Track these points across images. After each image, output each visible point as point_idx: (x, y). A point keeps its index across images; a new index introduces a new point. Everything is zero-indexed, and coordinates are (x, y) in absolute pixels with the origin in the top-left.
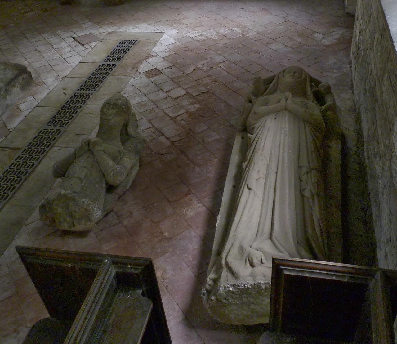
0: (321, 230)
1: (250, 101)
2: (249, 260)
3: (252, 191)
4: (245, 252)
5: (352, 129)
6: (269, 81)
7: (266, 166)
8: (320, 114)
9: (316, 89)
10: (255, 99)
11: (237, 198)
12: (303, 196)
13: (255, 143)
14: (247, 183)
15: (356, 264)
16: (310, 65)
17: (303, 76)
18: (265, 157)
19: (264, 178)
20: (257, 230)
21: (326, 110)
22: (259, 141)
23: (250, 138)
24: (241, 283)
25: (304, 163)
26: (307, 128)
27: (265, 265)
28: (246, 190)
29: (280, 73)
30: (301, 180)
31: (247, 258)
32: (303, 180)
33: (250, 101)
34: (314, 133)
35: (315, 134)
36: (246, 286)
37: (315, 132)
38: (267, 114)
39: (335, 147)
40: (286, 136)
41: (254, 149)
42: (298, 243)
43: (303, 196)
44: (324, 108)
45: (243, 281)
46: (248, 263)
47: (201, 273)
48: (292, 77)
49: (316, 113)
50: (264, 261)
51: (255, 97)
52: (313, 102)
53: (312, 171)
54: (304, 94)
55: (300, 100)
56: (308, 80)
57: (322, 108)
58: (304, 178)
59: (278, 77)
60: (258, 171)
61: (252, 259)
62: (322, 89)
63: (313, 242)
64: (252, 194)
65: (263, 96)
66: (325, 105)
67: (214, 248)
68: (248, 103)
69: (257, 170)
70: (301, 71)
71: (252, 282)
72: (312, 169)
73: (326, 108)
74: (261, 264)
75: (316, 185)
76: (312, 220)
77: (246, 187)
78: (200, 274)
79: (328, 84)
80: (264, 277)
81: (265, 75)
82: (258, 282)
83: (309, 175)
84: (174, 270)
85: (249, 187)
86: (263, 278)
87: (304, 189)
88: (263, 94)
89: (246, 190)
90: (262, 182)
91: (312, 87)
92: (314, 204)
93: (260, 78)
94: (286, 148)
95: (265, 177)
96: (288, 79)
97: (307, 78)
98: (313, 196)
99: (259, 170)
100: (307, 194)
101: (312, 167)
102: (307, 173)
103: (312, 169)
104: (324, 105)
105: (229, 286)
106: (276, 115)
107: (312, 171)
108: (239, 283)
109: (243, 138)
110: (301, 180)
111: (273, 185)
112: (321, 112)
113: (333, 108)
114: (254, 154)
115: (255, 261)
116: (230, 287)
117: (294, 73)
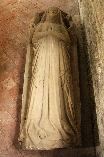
0: (72, 106)
2: (39, 135)
4: (37, 130)
5: (80, 35)
9: (64, 18)
14: (35, 84)
17: (58, 13)
20: (42, 108)
21: (71, 30)
25: (63, 68)
27: (47, 138)
31: (38, 134)
32: (63, 79)
33: (33, 26)
34: (65, 47)
37: (66, 46)
38: (42, 37)
42: (62, 119)
46: (38, 137)
47: (18, 120)
50: (46, 136)
54: (59, 22)
57: (68, 29)
58: (63, 78)
62: (68, 18)
64: (37, 89)
75: (69, 81)
77: (34, 85)
78: (18, 120)
80: (47, 145)
83: (65, 75)
84: (6, 119)
88: (39, 23)
90: (42, 82)
91: (62, 16)
94: (53, 58)
100: (65, 88)
102: (64, 74)
111: (47, 95)
113: (73, 29)
115: (42, 137)
117: (54, 11)
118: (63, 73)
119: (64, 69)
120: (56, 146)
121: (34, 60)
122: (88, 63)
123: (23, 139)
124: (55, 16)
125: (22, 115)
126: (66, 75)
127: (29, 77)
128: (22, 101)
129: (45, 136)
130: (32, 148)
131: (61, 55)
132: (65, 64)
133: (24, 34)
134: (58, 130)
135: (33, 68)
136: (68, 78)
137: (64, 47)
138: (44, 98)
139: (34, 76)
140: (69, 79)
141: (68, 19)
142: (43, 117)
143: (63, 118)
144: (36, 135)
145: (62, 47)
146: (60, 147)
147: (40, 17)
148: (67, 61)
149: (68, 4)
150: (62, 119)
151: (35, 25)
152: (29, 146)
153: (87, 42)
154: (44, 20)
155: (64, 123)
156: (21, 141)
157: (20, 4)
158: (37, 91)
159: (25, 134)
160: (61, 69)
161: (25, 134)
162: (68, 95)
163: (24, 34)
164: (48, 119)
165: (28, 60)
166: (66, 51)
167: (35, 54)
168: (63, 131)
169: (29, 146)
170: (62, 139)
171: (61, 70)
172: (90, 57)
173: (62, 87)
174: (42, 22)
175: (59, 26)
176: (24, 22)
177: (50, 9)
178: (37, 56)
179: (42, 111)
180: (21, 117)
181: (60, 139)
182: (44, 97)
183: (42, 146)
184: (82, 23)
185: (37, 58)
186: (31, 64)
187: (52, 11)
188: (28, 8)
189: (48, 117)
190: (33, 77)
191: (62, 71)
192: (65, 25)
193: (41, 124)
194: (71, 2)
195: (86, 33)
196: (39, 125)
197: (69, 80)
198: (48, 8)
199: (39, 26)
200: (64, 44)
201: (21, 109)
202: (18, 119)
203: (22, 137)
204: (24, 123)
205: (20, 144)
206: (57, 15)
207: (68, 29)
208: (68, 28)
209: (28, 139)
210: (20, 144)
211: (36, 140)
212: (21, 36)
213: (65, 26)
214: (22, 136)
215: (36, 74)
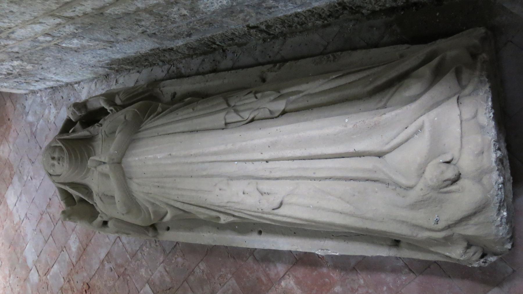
1: (105, 223)
3: (286, 200)
4: (428, 196)
6: (68, 198)
7: (231, 182)
8: (120, 113)
9: (78, 125)
10: (101, 217)
11: (295, 224)
12: (284, 113)
13: (186, 207)
14: (270, 210)
15: (79, 192)
16: (38, 147)
17: (60, 144)
18: (215, 185)
19: (257, 183)
22: (181, 199)
23: (174, 217)
24: (497, 195)
25: (219, 119)
26: (148, 126)
28: (284, 211)
29: (54, 181)
30: (252, 120)
31: (442, 190)
32: (252, 116)
33: (105, 223)
35: (160, 113)
36: (500, 186)
37: (155, 114)
39: (170, 88)
40: (170, 155)
41: (197, 206)
43: (284, 113)
44: (111, 108)
45: (494, 192)
46: (453, 187)
47: (410, 270)
48: (61, 162)
49: (122, 117)
50: (448, 159)
51: (97, 217)
52: (101, 125)
53: (233, 104)
54: (89, 140)
55: (98, 145)
56: (66, 137)
57: (111, 110)
58: (247, 115)
59: (59, 183)
60: (244, 193)
61: (445, 181)
63: (379, 82)
65: (95, 205)
66: (106, 107)
67: (383, 252)
68: (108, 227)
69: (243, 196)
70: (52, 148)
71: (495, 175)
72: (229, 105)
73: (110, 106)
74: (454, 162)
75: (259, 95)
76: (331, 90)
77: (276, 211)
79: (70, 107)
80: (483, 153)
81: (58, 205)
82: (494, 164)
85: (278, 206)
86: (485, 154)
87: (271, 112)
88: (92, 205)
89: (284, 211)
90: (265, 186)
92: (299, 92)
93: (63, 212)
95: (254, 181)
96: (64, 169)
97: (62, 137)
98: (281, 97)
99: (242, 193)
101: (226, 106)
102: (236, 112)
103: (229, 105)
104: (106, 110)
105: (499, 219)
106: (131, 178)
107: (233, 104)
108: (496, 200)
109: (168, 229)
110: (252, 120)
112: (117, 111)
113: (109, 97)
114: (208, 207)
115: (450, 174)
116: (502, 215)
117: (53, 158)
118: (233, 117)
119: (222, 115)
120: (486, 117)
121: (202, 217)
122: (215, 43)
123: (473, 250)
124: (70, 154)
125: (383, 252)
126: (241, 105)
127: (260, 233)
128: (337, 254)
129: (448, 162)
130: (499, 210)
131: (181, 126)
132: (205, 112)
133: (140, 255)
134: (424, 118)
135: (224, 219)
136: (250, 98)
137: (158, 119)
138: (315, 176)
139: (248, 213)
140: (251, 95)
141: (80, 114)
142: (380, 176)
143: (381, 101)
144: (447, 195)
145: (157, 126)
146: (490, 104)
147: (78, 204)
148: (199, 107)
149: (52, 118)
150: (385, 107)
151: (99, 219)
152: (493, 226)
153: (151, 50)
154: (86, 189)
155: (397, 98)
156: (479, 255)
157: (52, 269)
158: (294, 200)
159: (448, 241)
160: (223, 122)
161: (448, 241)
162: (301, 95)
163: (140, 255)
164: (387, 156)
165: (206, 237)
166: (171, 111)
167: (181, 212)
168: (426, 99)
169: (493, 226)
170: (455, 98)
171: (226, 124)
172: (194, 38)
173: (277, 115)
174: (92, 199)
175: (100, 142)
176: (103, 256)
177: (51, 172)
178: (186, 205)
179: (326, 179)
180: (397, 258)
181: (456, 104)
182: (310, 174)
183: (489, 171)
184: (101, 71)
185: (192, 207)
186: (220, 227)
187: (53, 165)
188: (64, 248)
189: (380, 155)
190: (245, 214)
191: (228, 121)
192: (98, 121)
193: (404, 181)
194: (47, 111)
195: (125, 56)
196: (411, 188)
197: (256, 93)
198: (47, 178)
199: (100, 206)
200: (153, 118)
201: (310, 253)
202: (407, 270)
203: (465, 253)
204: (414, 245)
205: (492, 259)
206: (68, 150)
207: (111, 110)
208: (109, 113)
209: (470, 230)
210: (492, 259)
211: (466, 196)
212: (144, 263)
213: (100, 122)
214: (456, 253)
215: (238, 207)
